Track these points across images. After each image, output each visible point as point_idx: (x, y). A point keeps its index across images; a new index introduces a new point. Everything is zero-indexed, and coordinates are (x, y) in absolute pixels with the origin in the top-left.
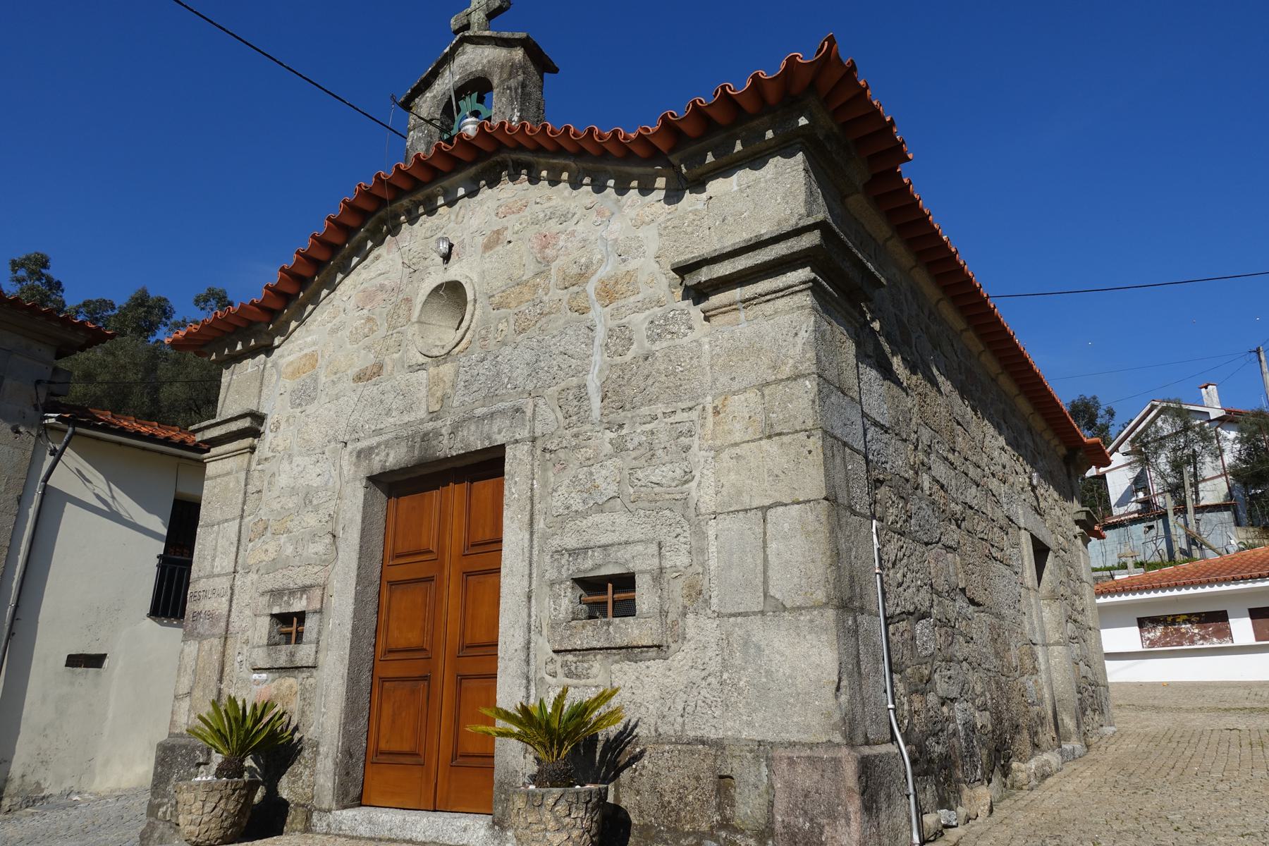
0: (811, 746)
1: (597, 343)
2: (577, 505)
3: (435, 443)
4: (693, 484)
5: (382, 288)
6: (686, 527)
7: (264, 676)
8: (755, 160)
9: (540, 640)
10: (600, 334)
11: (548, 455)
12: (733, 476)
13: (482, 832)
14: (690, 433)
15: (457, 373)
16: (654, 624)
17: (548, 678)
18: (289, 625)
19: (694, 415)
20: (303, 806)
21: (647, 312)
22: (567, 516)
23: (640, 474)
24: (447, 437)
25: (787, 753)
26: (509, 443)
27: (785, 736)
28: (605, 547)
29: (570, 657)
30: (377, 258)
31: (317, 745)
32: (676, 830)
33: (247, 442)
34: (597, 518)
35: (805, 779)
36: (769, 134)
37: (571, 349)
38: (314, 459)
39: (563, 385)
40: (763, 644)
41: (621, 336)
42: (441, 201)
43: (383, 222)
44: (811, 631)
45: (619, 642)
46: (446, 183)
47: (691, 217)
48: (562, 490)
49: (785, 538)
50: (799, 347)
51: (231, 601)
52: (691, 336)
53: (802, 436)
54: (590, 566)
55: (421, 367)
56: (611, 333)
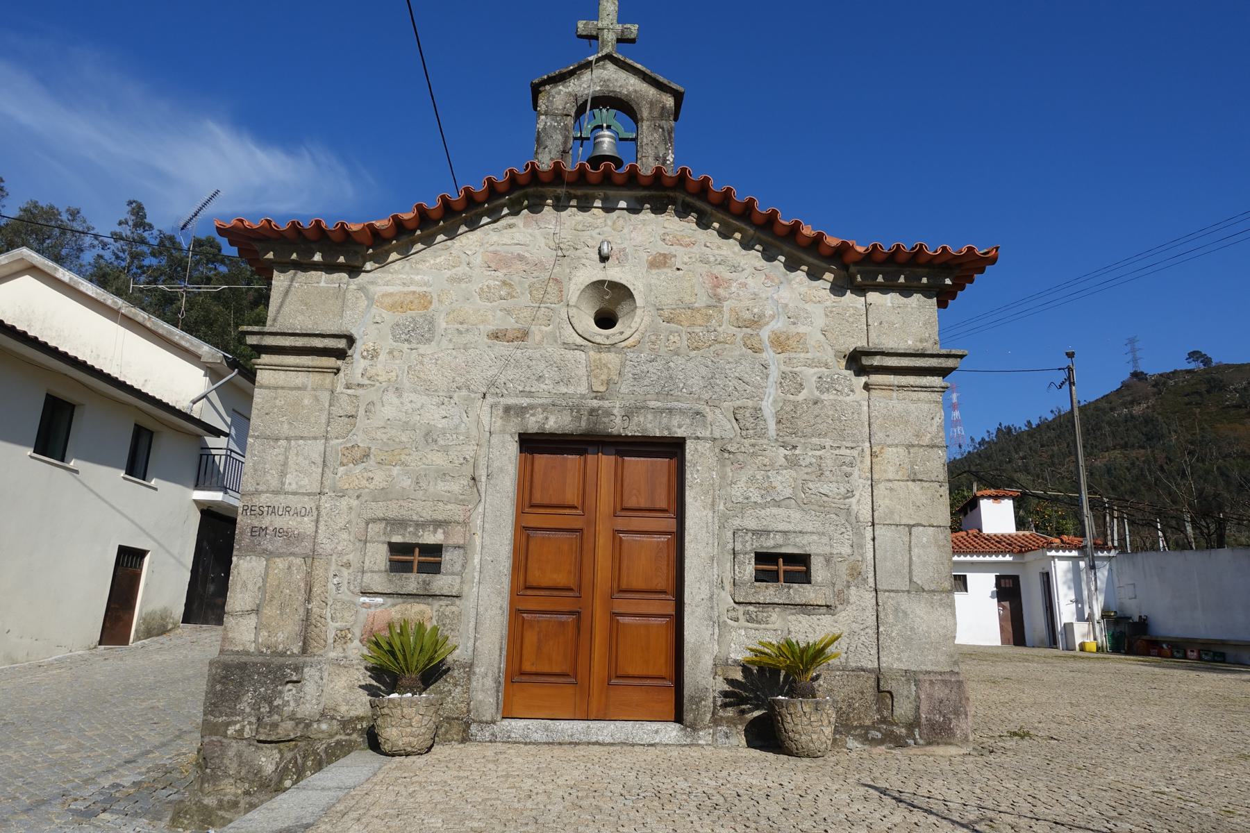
0: (941, 673)
1: (771, 379)
2: (755, 496)
3: (606, 420)
4: (854, 500)
5: (521, 258)
6: (849, 529)
7: (379, 600)
8: (906, 291)
9: (723, 594)
10: (774, 374)
11: (726, 455)
12: (887, 501)
13: (674, 733)
14: (851, 465)
15: (623, 365)
16: (828, 591)
17: (729, 622)
18: (415, 558)
19: (855, 453)
20: (457, 719)
21: (816, 369)
22: (744, 506)
23: (810, 485)
24: (619, 418)
25: (926, 677)
26: (690, 438)
27: (924, 668)
28: (785, 533)
29: (751, 608)
30: (511, 226)
31: (469, 667)
32: (847, 725)
33: (331, 362)
34: (775, 510)
35: (940, 692)
36: (925, 280)
37: (746, 377)
38: (435, 400)
39: (739, 403)
40: (909, 611)
41: (791, 381)
42: (598, 203)
43: (526, 197)
44: (941, 605)
45: (798, 601)
46: (611, 193)
47: (852, 311)
48: (741, 484)
49: (924, 546)
50: (934, 428)
51: (317, 521)
52: (852, 397)
53: (937, 485)
54: (769, 544)
55: (579, 347)
56: (784, 376)
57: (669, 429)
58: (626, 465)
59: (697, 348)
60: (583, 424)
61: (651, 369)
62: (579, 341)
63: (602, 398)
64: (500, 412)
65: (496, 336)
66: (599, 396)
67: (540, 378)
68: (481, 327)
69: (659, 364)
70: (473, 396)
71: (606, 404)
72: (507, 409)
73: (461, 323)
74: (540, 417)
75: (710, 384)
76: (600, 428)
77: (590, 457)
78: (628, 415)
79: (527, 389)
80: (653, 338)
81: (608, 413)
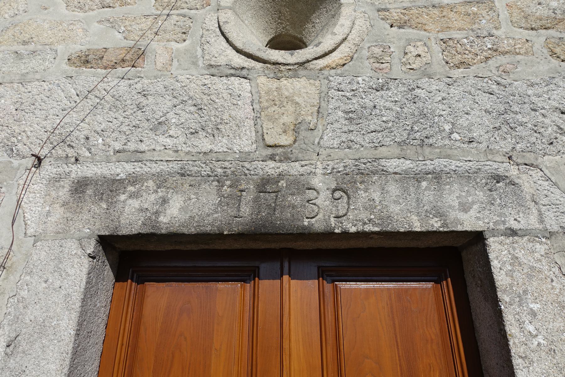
3: (296, 200)
15: (324, 96)
26: (495, 233)
57: (440, 215)
58: (343, 299)
59: (462, 64)
60: (246, 210)
61: (381, 103)
62: (239, 60)
63: (286, 158)
64: (64, 193)
65: (84, 61)
66: (275, 152)
67: (159, 126)
68: (60, 48)
69: (396, 92)
70: (16, 162)
71: (295, 168)
72: (80, 187)
73: (25, 43)
74: (150, 200)
75: (504, 122)
76: (284, 219)
77: (267, 286)
78: (343, 189)
79: (132, 146)
80: (377, 51)
81: (302, 186)
